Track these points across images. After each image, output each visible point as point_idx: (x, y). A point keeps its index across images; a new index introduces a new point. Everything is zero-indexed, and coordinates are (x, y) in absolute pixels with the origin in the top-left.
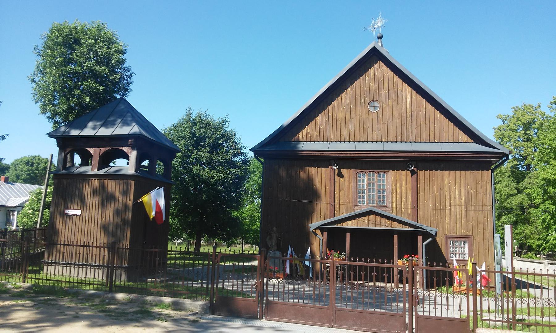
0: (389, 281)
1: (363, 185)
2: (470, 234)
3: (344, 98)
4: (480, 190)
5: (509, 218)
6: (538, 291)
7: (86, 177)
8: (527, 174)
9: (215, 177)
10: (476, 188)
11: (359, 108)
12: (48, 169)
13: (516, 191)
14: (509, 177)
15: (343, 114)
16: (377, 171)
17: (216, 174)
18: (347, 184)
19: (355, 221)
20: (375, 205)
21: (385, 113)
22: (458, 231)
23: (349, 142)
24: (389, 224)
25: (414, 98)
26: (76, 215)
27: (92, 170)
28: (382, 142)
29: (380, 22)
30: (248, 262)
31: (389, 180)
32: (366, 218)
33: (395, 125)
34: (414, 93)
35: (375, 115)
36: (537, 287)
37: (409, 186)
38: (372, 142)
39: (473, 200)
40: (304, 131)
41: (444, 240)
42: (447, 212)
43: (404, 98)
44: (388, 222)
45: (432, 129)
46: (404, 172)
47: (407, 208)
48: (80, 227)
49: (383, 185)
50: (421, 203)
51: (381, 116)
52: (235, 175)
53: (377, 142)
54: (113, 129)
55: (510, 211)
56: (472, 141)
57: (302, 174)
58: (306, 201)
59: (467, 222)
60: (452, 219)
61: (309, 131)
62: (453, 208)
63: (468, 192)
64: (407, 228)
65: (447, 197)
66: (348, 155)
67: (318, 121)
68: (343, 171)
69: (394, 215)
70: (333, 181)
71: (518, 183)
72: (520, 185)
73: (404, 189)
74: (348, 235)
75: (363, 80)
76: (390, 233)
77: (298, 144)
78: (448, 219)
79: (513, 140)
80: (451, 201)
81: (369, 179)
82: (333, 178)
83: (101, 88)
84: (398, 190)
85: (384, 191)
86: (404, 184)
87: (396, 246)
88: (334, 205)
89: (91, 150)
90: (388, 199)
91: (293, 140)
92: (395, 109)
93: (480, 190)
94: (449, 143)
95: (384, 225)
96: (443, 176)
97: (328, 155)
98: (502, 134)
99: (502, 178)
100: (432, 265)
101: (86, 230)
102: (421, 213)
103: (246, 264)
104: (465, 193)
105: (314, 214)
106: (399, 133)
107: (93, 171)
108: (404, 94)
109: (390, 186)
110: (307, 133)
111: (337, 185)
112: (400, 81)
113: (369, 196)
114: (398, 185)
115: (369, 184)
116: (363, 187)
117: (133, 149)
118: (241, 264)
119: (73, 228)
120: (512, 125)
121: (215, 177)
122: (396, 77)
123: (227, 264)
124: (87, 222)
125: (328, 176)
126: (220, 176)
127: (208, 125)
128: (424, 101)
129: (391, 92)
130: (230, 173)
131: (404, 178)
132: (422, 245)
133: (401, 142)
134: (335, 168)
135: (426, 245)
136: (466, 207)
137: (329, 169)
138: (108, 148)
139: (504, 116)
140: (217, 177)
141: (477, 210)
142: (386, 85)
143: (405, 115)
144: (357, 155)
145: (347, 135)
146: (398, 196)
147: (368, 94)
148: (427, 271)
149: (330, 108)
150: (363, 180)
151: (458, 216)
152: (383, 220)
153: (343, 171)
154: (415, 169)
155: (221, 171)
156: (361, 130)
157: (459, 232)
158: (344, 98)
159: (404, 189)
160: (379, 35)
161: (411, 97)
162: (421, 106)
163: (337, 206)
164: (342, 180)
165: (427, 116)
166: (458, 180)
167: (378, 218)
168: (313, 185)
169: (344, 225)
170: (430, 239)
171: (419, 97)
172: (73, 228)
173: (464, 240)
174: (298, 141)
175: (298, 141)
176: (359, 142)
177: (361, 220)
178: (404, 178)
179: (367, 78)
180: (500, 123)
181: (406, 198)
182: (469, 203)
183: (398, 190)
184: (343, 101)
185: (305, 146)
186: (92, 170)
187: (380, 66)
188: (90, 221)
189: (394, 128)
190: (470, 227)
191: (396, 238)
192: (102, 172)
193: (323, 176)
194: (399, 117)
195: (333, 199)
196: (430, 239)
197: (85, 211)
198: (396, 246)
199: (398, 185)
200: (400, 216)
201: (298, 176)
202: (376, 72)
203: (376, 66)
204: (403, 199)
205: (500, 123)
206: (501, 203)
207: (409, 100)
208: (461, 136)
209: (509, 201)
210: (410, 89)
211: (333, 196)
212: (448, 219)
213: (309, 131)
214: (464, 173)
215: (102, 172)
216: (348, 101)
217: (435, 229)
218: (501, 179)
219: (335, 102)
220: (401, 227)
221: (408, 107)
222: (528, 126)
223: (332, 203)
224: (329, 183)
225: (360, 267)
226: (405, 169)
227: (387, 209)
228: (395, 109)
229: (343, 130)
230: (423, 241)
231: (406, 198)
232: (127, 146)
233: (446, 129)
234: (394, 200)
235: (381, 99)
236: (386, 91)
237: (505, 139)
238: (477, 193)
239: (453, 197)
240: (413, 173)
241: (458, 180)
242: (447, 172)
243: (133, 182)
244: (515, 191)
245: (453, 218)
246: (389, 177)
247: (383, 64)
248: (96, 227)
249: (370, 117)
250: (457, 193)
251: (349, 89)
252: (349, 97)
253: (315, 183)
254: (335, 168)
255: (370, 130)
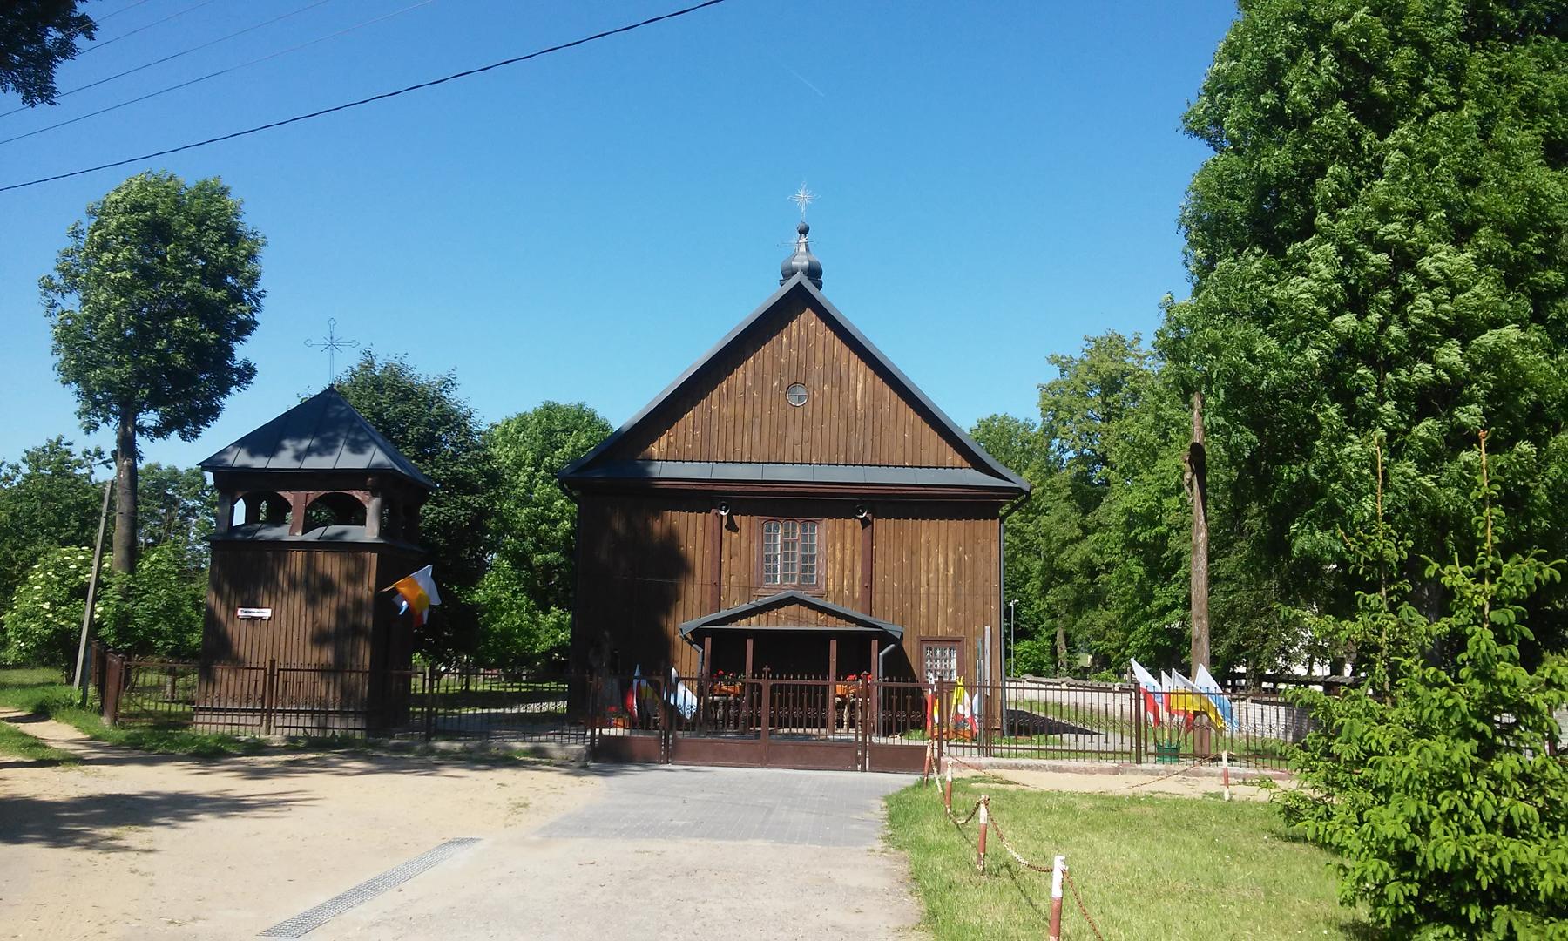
0: (823, 727)
1: (775, 546)
2: (961, 634)
3: (740, 377)
4: (979, 554)
5: (1065, 592)
6: (1088, 737)
7: (281, 547)
8: (1105, 494)
9: (428, 515)
10: (973, 551)
11: (769, 398)
12: (104, 515)
13: (1080, 531)
14: (1067, 499)
15: (739, 408)
16: (801, 520)
17: (431, 509)
18: (744, 544)
19: (763, 617)
20: (796, 583)
21: (818, 408)
22: (941, 629)
23: (750, 463)
24: (822, 621)
25: (869, 381)
26: (261, 618)
27: (292, 533)
28: (810, 464)
29: (803, 197)
30: (497, 708)
31: (823, 537)
32: (782, 611)
33: (834, 432)
34: (871, 372)
35: (799, 412)
36: (1087, 732)
37: (859, 547)
38: (793, 464)
39: (968, 572)
40: (663, 440)
41: (915, 646)
42: (924, 597)
43: (852, 382)
44: (821, 617)
45: (901, 441)
46: (849, 522)
47: (853, 593)
48: (270, 641)
49: (812, 547)
50: (878, 580)
51: (810, 414)
52: (475, 509)
53: (801, 464)
54: (334, 458)
55: (1067, 576)
56: (969, 465)
57: (657, 526)
58: (667, 581)
59: (956, 612)
60: (931, 609)
61: (672, 439)
62: (932, 589)
63: (960, 559)
64: (853, 627)
65: (924, 567)
66: (749, 489)
67: (691, 420)
68: (737, 518)
69: (829, 604)
70: (718, 538)
71: (1085, 513)
72: (1089, 518)
73: (848, 552)
74: (750, 643)
75: (777, 342)
76: (823, 638)
77: (649, 465)
78: (923, 609)
79: (1078, 417)
80: (931, 576)
81: (787, 535)
82: (717, 532)
83: (213, 335)
84: (838, 555)
85: (812, 557)
86: (848, 545)
87: (833, 660)
88: (718, 585)
89: (288, 496)
90: (820, 572)
91: (640, 457)
92: (835, 401)
93: (979, 554)
94: (929, 467)
95: (815, 623)
96: (917, 529)
97: (710, 488)
98: (1056, 403)
99: (1054, 501)
100: (891, 680)
101: (282, 645)
102: (878, 598)
103: (508, 711)
104: (955, 560)
105: (680, 603)
106: (842, 448)
107: (294, 535)
108: (852, 374)
109: (823, 548)
110: (669, 444)
111: (725, 545)
112: (846, 349)
113: (785, 567)
114: (838, 545)
115: (786, 545)
116: (775, 550)
117: (374, 494)
118: (500, 711)
119: (256, 642)
120: (1077, 382)
121: (428, 515)
122: (838, 342)
123: (464, 711)
124: (284, 631)
125: (709, 529)
126: (440, 513)
127: (408, 394)
128: (887, 389)
129: (828, 367)
130: (466, 505)
131: (849, 532)
132: (878, 656)
133: (846, 465)
134: (723, 513)
135: (884, 656)
136: (955, 585)
137: (710, 516)
138: (323, 493)
139: (1062, 358)
140: (432, 516)
141: (973, 594)
142: (820, 355)
143: (854, 414)
144: (765, 489)
145: (745, 449)
146: (838, 566)
147: (786, 371)
148: (884, 688)
149: (715, 394)
150: (775, 536)
151: (941, 601)
152: (812, 614)
153: (737, 518)
154: (870, 516)
155: (442, 502)
156: (774, 440)
157: (942, 631)
158: (741, 375)
159: (848, 552)
160: (802, 226)
161: (865, 382)
162: (882, 398)
163: (725, 589)
164: (735, 536)
165: (893, 417)
166: (943, 537)
167: (804, 610)
168: (679, 547)
169: (743, 625)
170: (892, 646)
171: (879, 380)
172: (256, 642)
173: (951, 645)
174: (650, 460)
175: (650, 460)
176: (768, 463)
177: (773, 614)
178: (849, 532)
179: (785, 339)
180: (1054, 373)
181: (852, 570)
182: (960, 578)
183: (838, 555)
184: (739, 383)
185: (664, 470)
186: (292, 533)
187: (808, 319)
188: (290, 628)
189: (834, 438)
190: (961, 621)
191: (833, 644)
192: (313, 536)
193: (699, 528)
194: (842, 417)
195: (717, 572)
196: (892, 646)
197: (278, 610)
198: (833, 660)
199: (838, 545)
200: (840, 605)
201: (648, 530)
202: (802, 329)
203: (802, 317)
204: (847, 572)
205: (1054, 373)
206: (1050, 560)
207: (860, 386)
208: (952, 456)
209: (1064, 555)
210: (862, 365)
211: (717, 568)
212: (923, 609)
213: (672, 439)
214: (953, 523)
215: (313, 536)
216: (749, 384)
217: (900, 628)
218: (1050, 504)
219: (724, 384)
220: (842, 626)
221: (859, 399)
222: (1111, 385)
223: (717, 580)
224: (710, 539)
225: (802, 686)
226: (851, 514)
227: (817, 591)
228: (835, 401)
229: (738, 441)
230: (879, 652)
231: (852, 570)
232: (364, 488)
233: (925, 443)
234: (830, 573)
235: (810, 381)
236: (819, 368)
237: (1061, 414)
238: (974, 560)
239: (933, 567)
240: (865, 523)
241: (943, 537)
242: (925, 522)
243: (375, 556)
244: (1078, 532)
245: (932, 605)
246: (823, 530)
247: (814, 315)
248: (301, 641)
249: (791, 416)
250: (941, 560)
251: (751, 360)
252: (750, 374)
253: (683, 540)
254: (723, 513)
255: (789, 441)
